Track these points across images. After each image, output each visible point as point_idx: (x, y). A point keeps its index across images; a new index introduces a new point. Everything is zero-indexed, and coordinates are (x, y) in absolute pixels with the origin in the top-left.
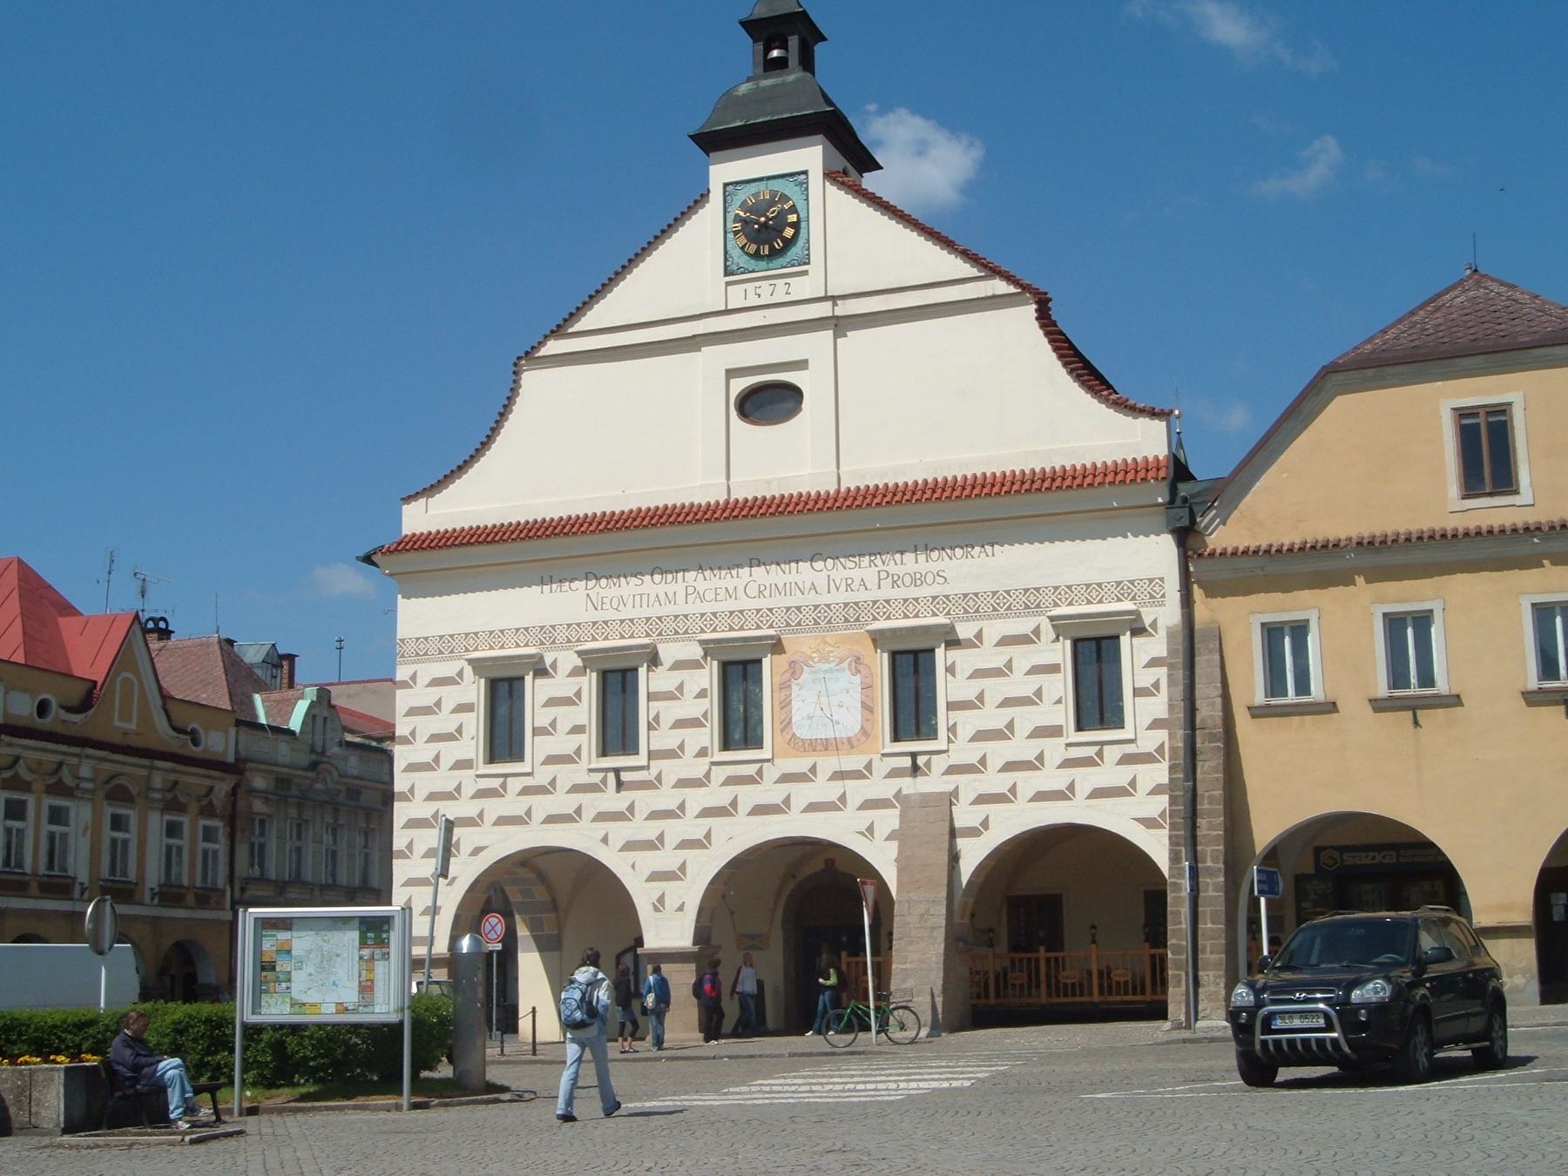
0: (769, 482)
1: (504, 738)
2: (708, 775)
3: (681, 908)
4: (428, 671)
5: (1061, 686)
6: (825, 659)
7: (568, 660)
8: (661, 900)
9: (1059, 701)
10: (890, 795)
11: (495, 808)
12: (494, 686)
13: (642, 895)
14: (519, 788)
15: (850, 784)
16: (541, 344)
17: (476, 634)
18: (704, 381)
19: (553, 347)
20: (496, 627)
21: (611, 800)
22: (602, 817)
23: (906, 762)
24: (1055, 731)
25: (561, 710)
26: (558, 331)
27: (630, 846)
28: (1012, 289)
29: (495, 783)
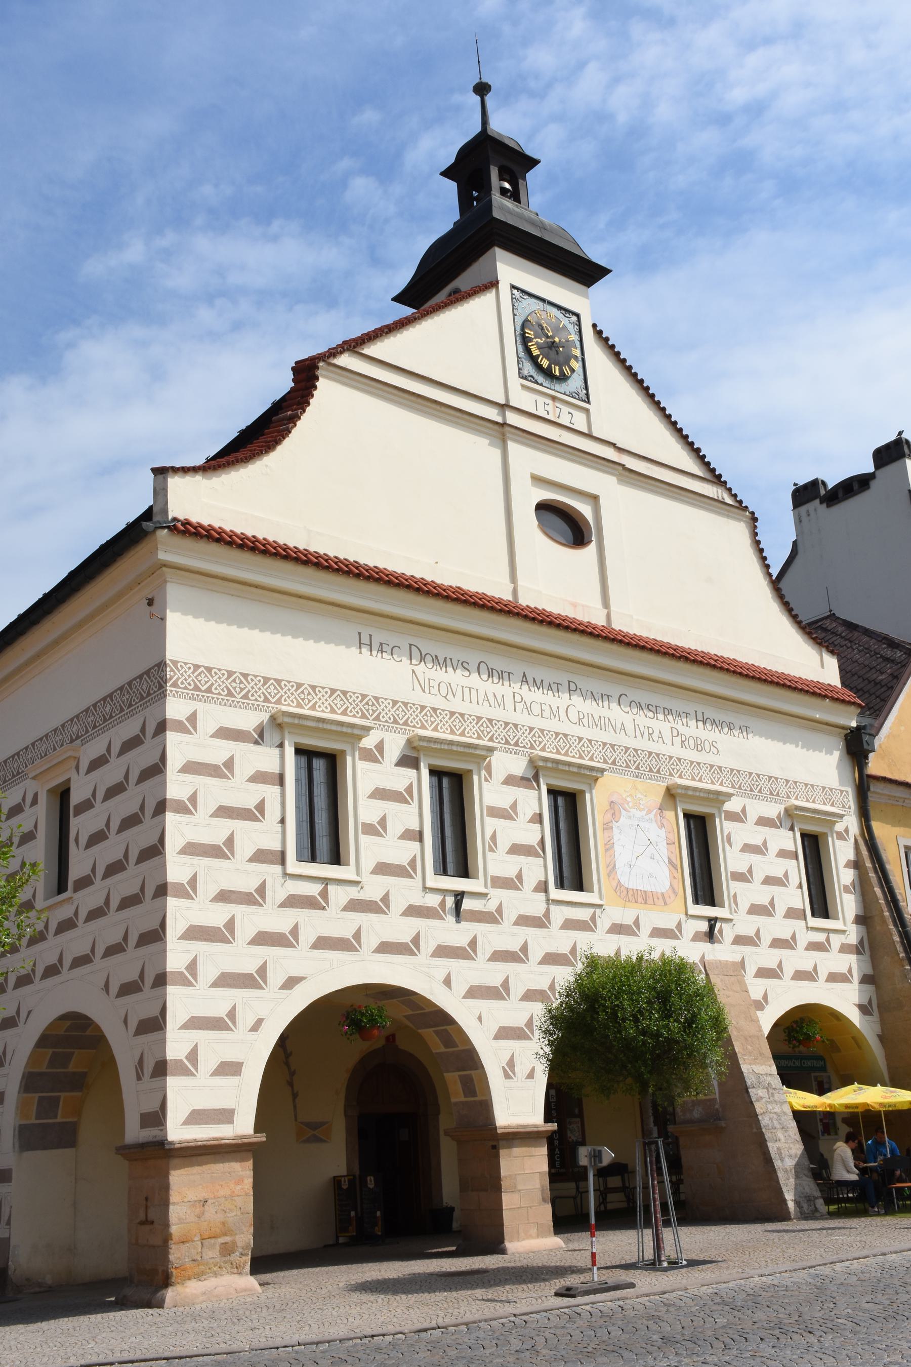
0: (575, 605)
1: (324, 833)
2: (547, 914)
4: (213, 715)
8: (511, 1063)
11: (313, 924)
13: (492, 1055)
14: (344, 901)
17: (279, 681)
19: (345, 360)
20: (307, 679)
22: (443, 951)
23: (704, 926)
25: (386, 806)
26: (353, 346)
27: (475, 992)
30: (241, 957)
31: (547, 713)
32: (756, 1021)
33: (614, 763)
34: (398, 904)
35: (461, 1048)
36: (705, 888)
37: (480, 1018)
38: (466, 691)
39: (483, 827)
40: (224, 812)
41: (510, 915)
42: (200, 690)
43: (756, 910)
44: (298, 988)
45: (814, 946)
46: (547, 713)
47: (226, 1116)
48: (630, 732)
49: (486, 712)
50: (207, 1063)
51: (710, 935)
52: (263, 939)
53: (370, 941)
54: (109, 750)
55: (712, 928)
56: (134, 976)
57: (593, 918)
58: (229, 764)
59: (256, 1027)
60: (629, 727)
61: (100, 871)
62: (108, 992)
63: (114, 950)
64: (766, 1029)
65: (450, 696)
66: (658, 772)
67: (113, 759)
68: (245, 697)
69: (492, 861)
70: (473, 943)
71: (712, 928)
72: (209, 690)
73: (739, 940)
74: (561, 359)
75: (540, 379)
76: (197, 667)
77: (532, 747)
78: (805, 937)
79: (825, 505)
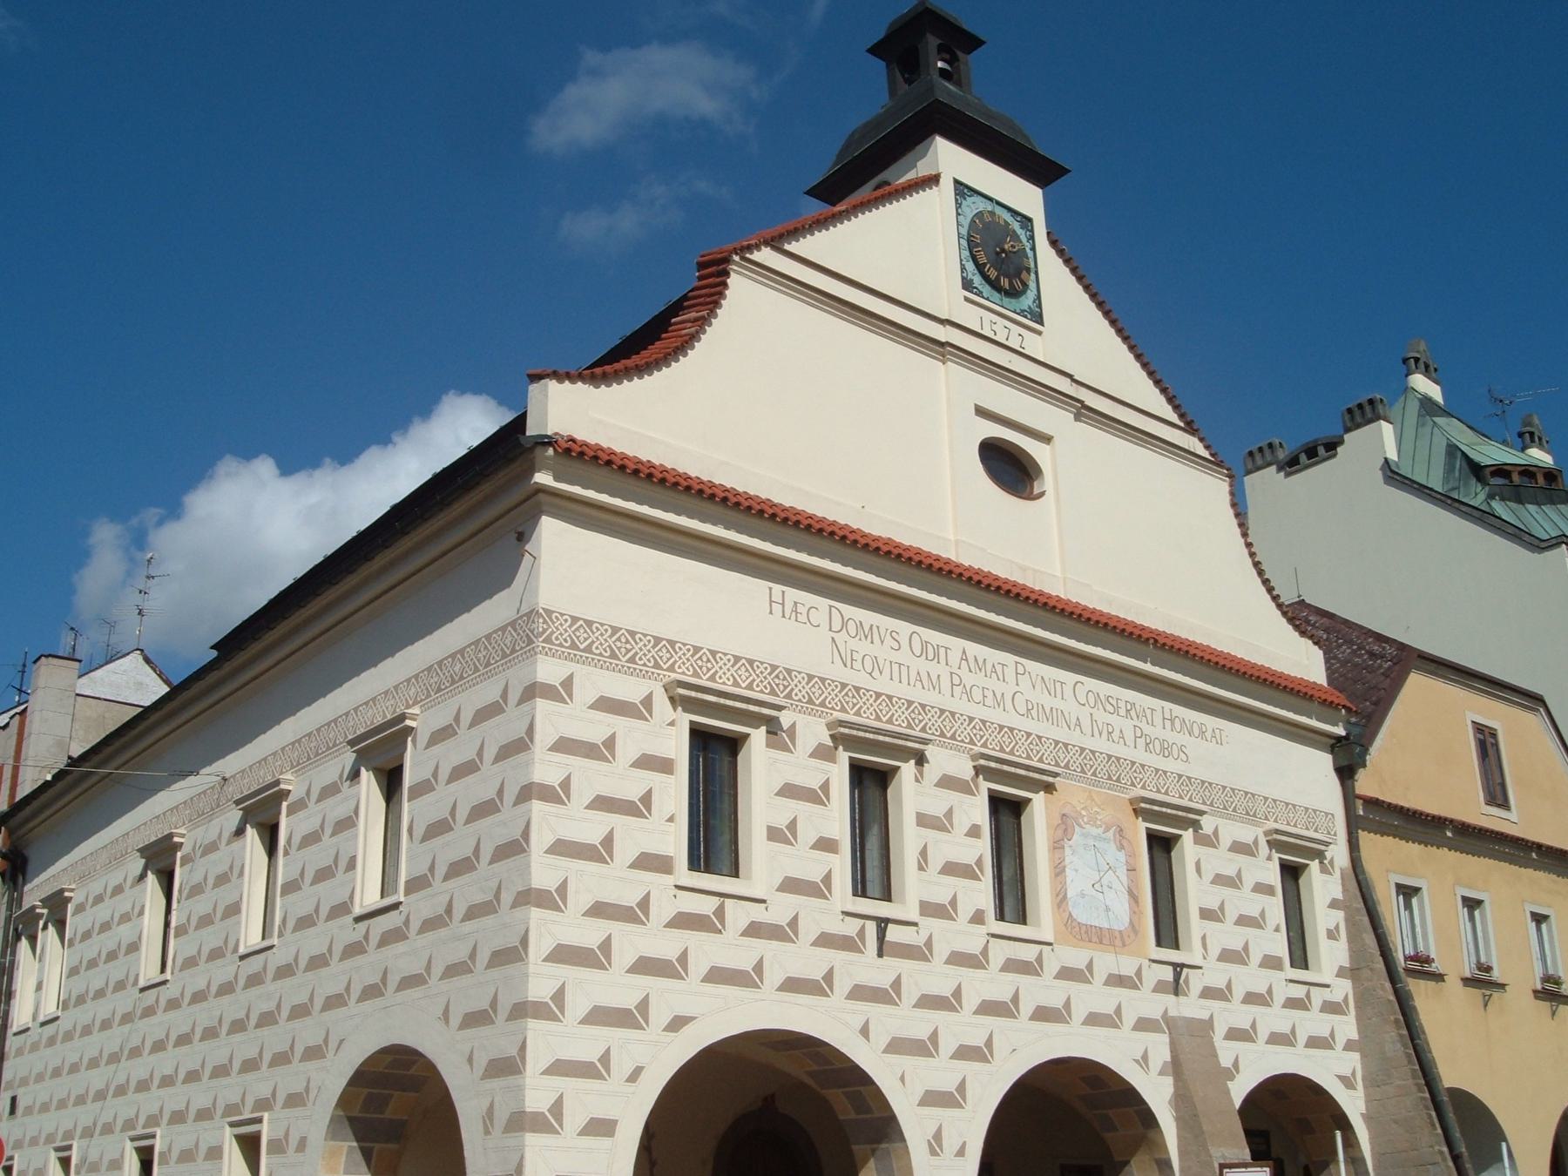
0: (1024, 569)
2: (985, 951)
3: (961, 1152)
4: (594, 682)
6: (1093, 821)
7: (812, 731)
8: (938, 1136)
9: (671, 819)
10: (1156, 1014)
11: (706, 951)
12: (701, 739)
14: (743, 924)
16: (758, 247)
17: (672, 643)
18: (948, 410)
19: (765, 256)
20: (708, 643)
21: (870, 969)
22: (860, 993)
24: (660, 864)
26: (776, 243)
27: (897, 1046)
28: (1206, 454)
29: (707, 906)
30: (618, 988)
31: (989, 701)
32: (1227, 1092)
33: (1066, 767)
34: (808, 931)
35: (877, 1114)
36: (1167, 930)
37: (902, 1079)
38: (895, 667)
39: (908, 838)
40: (603, 803)
41: (941, 951)
42: (578, 649)
43: (1227, 956)
44: (687, 1030)
45: (1293, 1003)
46: (989, 701)
48: (1087, 730)
49: (918, 695)
50: (574, 1118)
51: (1176, 988)
52: (645, 966)
53: (774, 976)
54: (457, 719)
55: (1177, 976)
56: (484, 1004)
57: (1039, 959)
58: (610, 743)
60: (1086, 723)
61: (441, 870)
62: (447, 1022)
63: (455, 970)
64: (1238, 1103)
65: (876, 674)
66: (1118, 780)
67: (462, 731)
68: (632, 660)
69: (915, 884)
70: (897, 985)
71: (1177, 976)
72: (588, 649)
73: (1208, 993)
74: (1012, 271)
75: (987, 290)
76: (575, 619)
77: (972, 742)
78: (1283, 992)
79: (1282, 474)
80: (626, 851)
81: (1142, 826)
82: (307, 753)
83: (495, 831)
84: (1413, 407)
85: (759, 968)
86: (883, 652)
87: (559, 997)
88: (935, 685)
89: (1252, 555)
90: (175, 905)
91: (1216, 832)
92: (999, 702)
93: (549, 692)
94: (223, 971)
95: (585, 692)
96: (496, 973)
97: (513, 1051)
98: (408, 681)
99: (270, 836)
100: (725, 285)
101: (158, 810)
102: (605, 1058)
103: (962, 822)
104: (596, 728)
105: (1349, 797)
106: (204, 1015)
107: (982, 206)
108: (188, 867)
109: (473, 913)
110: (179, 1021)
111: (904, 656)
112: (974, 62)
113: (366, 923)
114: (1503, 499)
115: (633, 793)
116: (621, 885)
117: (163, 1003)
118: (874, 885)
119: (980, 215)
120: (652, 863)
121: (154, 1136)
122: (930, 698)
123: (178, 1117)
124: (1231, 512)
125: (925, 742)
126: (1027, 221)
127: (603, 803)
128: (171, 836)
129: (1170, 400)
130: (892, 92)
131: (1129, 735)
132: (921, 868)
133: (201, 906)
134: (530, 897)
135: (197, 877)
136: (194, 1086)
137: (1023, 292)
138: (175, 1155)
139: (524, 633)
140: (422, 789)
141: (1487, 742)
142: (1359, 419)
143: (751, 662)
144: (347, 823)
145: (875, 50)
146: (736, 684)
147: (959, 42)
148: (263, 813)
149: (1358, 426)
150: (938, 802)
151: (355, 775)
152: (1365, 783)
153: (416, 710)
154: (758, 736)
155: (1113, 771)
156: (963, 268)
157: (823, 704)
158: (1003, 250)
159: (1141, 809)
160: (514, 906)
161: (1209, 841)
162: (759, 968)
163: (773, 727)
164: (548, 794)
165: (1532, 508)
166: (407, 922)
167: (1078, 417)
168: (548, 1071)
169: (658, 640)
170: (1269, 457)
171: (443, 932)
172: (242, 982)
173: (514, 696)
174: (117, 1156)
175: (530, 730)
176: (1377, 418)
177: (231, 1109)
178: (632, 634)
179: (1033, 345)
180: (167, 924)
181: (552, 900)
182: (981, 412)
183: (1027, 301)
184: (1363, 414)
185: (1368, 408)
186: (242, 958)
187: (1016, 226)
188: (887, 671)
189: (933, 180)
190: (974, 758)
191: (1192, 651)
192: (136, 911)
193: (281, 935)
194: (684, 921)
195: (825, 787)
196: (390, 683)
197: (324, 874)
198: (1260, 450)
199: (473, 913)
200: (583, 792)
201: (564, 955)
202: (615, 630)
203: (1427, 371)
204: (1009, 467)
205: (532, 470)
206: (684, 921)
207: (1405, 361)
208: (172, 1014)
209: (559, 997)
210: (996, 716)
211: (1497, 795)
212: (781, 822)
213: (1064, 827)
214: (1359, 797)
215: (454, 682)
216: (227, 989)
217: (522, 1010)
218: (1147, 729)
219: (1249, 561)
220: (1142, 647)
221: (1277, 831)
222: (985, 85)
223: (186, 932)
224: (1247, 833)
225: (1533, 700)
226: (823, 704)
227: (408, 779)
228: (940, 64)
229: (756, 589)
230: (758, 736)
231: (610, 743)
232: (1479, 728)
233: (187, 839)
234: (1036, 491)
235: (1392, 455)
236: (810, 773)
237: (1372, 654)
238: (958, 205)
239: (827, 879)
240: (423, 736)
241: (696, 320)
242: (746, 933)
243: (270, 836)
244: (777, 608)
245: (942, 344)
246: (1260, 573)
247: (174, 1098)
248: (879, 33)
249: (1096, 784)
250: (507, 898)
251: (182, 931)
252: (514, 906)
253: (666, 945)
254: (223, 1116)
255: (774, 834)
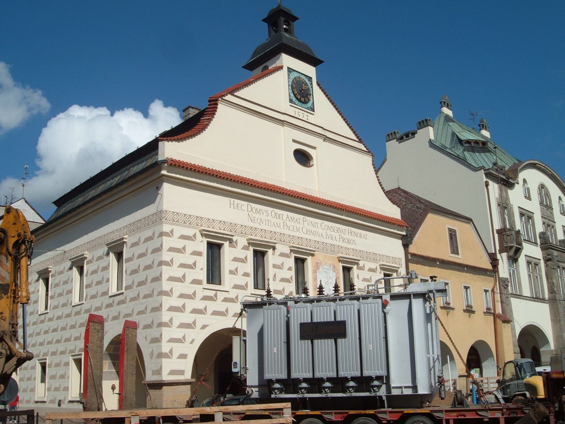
0: (306, 189)
4: (179, 231)
5: (202, 262)
6: (326, 264)
7: (242, 241)
9: (202, 269)
11: (212, 306)
12: (210, 245)
14: (223, 298)
15: (186, 301)
16: (227, 95)
17: (201, 218)
18: (285, 141)
19: (229, 97)
20: (212, 217)
24: (199, 282)
26: (232, 93)
28: (365, 149)
29: (212, 293)
39: (270, 272)
40: (182, 266)
47: (182, 372)
48: (325, 237)
49: (273, 229)
50: (176, 354)
52: (195, 311)
54: (139, 240)
58: (184, 248)
59: (192, 342)
60: (324, 234)
72: (177, 221)
75: (297, 102)
76: (174, 213)
77: (290, 242)
80: (189, 279)
81: (341, 265)
82: (92, 246)
83: (151, 274)
84: (442, 118)
85: (227, 310)
86: (263, 217)
87: (171, 320)
88: (279, 226)
89: (378, 180)
90: (49, 289)
91: (364, 266)
92: (298, 230)
93: (167, 234)
94: (67, 310)
95: (177, 234)
96: (153, 314)
97: (158, 336)
98: (124, 227)
99: (81, 270)
100: (217, 108)
101: (42, 260)
102: (184, 337)
103: (286, 266)
104: (180, 244)
105: (407, 253)
106: (61, 323)
107: (296, 75)
108: (54, 278)
109: (145, 297)
110: (53, 325)
111: (269, 218)
112: (296, 24)
113: (113, 298)
114: (468, 151)
115: (191, 262)
116: (188, 288)
117: (47, 319)
118: (260, 286)
119: (295, 78)
120: (196, 282)
121: (46, 359)
122: (277, 230)
123: (54, 354)
124: (372, 167)
125: (275, 243)
126: (310, 79)
127: (182, 266)
128: (48, 268)
129: (354, 133)
130: (270, 35)
131: (338, 238)
132: (274, 280)
133: (59, 290)
134: (162, 293)
135: (57, 281)
136: (59, 344)
137: (309, 102)
138: (54, 364)
139: (159, 217)
140: (129, 260)
141: (452, 235)
142: (422, 126)
143: (224, 222)
144: (106, 268)
145: (264, 20)
146: (220, 229)
147: (291, 18)
148: (79, 264)
149: (422, 128)
150: (279, 260)
151: (108, 254)
152: (412, 249)
153: (126, 236)
154: (226, 244)
155: (333, 248)
156: (290, 96)
157: (245, 234)
158: (302, 89)
159: (340, 260)
160: (158, 295)
161: (362, 269)
162: (227, 310)
163: (231, 241)
164: (167, 264)
165: (477, 154)
166: (126, 298)
167: (324, 141)
168: (168, 341)
169: (197, 217)
170: (394, 136)
171: (136, 302)
172: (73, 314)
173: (156, 235)
174: (34, 365)
175: (162, 245)
176: (428, 125)
177: (71, 351)
178: (190, 216)
179: (311, 119)
180: (47, 295)
181: (168, 294)
182: (294, 141)
183: (310, 104)
184: (423, 124)
185: (425, 122)
186: (73, 306)
187: (307, 81)
188: (264, 223)
189: (281, 68)
190: (290, 247)
191: (357, 212)
192: (36, 291)
193: (86, 300)
194: (205, 298)
195: (246, 258)
196: (119, 227)
197: (99, 283)
198: (391, 134)
199: (145, 297)
200: (176, 263)
201: (172, 309)
202: (185, 215)
203: (448, 106)
204: (303, 157)
205: (161, 170)
206: (205, 298)
207: (441, 103)
208: (50, 323)
209: (171, 320)
210: (297, 234)
211: (455, 250)
212: (233, 269)
213: (317, 266)
214: (409, 253)
215: (138, 229)
216: (68, 316)
217: (161, 325)
218: (343, 236)
219: (377, 182)
220: (342, 212)
221: (383, 265)
222: (300, 34)
223: (54, 298)
224: (373, 266)
225: (468, 220)
226: (245, 234)
227: (125, 257)
228: (284, 27)
229: (226, 200)
230: (226, 244)
231: (184, 248)
232: (450, 230)
233: (53, 269)
234: (311, 164)
235: (432, 138)
236: (241, 254)
237: (417, 207)
238: (289, 75)
239: (246, 285)
240: (129, 244)
241: (208, 119)
242: (223, 301)
243: (81, 270)
244: (232, 206)
245: (283, 121)
246: (381, 185)
247: (53, 348)
248: (266, 16)
249: (327, 253)
250: (156, 293)
251: (52, 297)
252: (158, 295)
253: (201, 305)
254: (69, 353)
255: (231, 272)
